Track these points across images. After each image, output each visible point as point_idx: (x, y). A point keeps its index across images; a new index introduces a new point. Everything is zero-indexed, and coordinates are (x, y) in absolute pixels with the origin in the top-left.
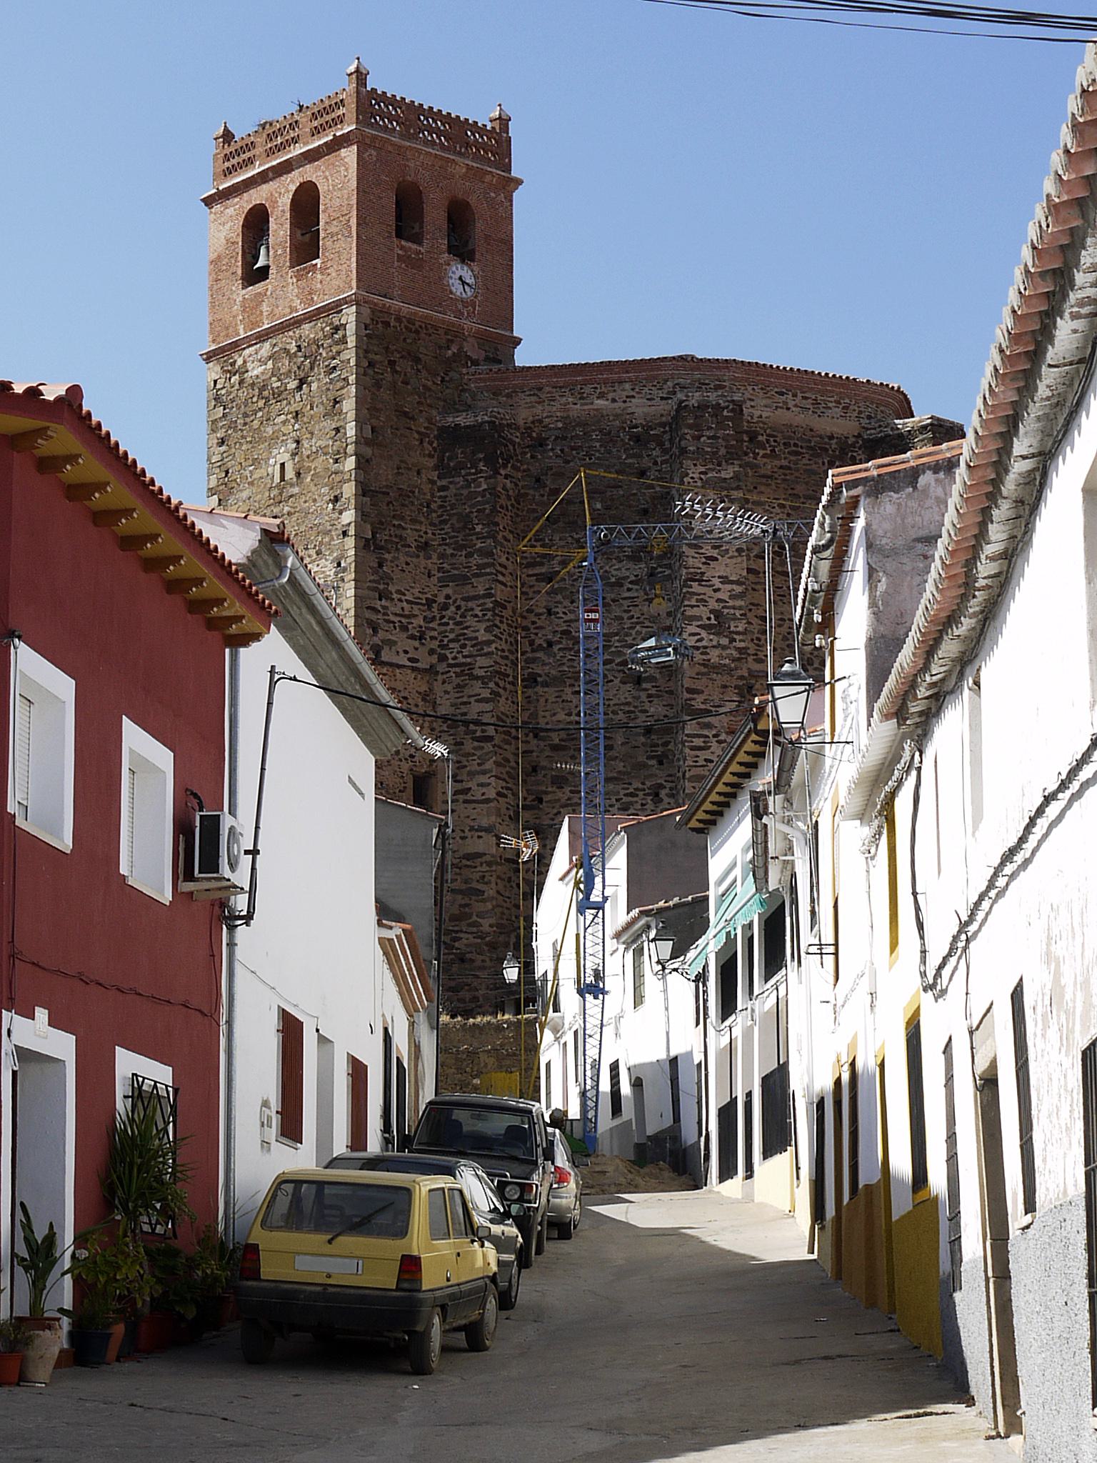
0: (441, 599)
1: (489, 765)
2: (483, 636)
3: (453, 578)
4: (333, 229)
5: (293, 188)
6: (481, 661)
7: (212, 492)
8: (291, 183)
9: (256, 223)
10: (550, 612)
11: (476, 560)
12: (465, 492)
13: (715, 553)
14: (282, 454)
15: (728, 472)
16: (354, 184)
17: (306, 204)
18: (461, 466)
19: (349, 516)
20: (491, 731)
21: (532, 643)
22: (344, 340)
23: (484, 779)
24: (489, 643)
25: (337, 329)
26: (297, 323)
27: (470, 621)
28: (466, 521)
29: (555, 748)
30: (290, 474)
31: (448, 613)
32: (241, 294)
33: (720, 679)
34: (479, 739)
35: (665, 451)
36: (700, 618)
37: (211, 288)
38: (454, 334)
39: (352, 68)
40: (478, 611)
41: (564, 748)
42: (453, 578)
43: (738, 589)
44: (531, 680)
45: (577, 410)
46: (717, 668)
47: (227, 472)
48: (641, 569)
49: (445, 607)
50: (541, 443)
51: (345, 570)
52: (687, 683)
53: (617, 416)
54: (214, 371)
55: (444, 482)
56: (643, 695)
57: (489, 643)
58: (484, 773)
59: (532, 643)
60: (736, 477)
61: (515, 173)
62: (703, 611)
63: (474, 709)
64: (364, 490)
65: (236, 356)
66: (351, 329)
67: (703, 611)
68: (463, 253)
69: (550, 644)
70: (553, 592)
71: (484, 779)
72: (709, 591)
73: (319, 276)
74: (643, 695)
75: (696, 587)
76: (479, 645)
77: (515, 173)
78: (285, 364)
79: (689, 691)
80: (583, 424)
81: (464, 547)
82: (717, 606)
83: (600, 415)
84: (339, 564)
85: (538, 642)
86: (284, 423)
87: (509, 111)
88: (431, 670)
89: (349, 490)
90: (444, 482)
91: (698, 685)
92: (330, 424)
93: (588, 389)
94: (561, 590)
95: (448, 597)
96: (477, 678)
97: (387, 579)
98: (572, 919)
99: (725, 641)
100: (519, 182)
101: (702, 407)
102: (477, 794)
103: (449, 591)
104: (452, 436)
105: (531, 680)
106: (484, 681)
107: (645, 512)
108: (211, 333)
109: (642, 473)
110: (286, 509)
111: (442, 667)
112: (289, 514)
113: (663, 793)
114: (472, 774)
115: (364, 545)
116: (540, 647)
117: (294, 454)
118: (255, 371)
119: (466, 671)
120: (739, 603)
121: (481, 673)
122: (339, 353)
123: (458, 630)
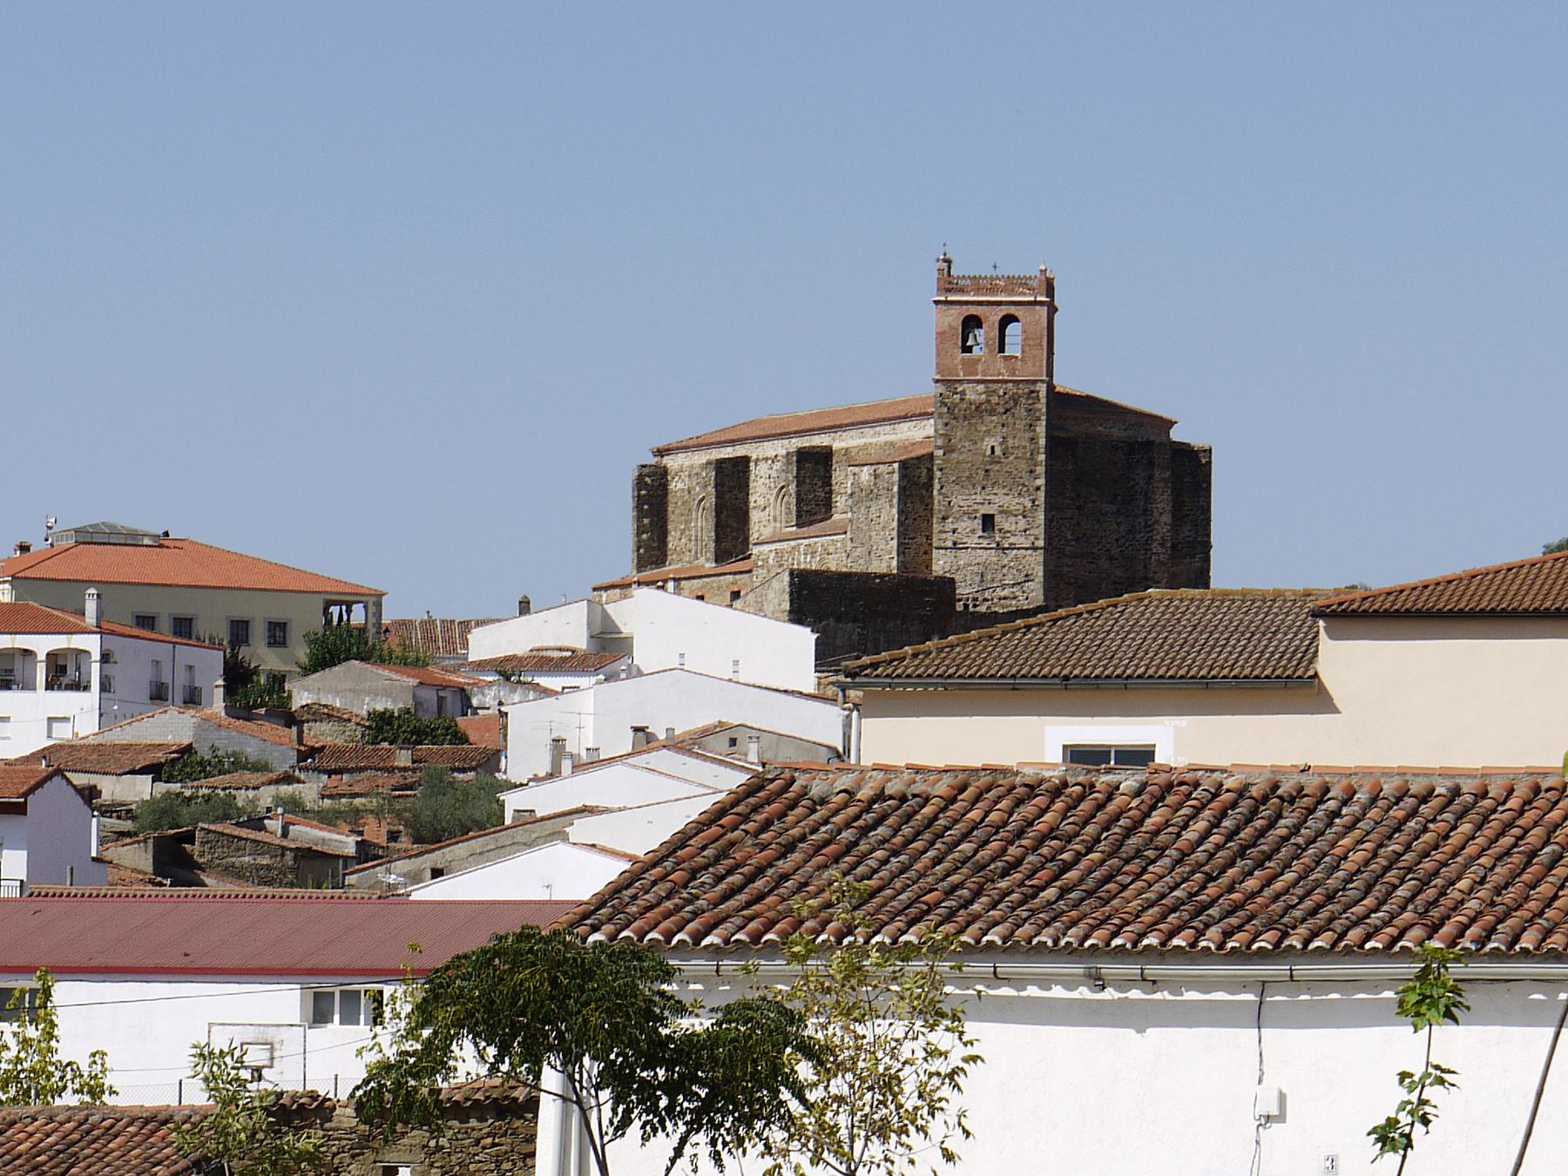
8: (1004, 311)
9: (972, 323)
11: (1067, 501)
19: (1041, 482)
22: (1038, 398)
26: (1006, 382)
30: (998, 452)
45: (1091, 430)
48: (1113, 508)
54: (941, 389)
89: (1041, 470)
92: (1028, 435)
118: (970, 396)
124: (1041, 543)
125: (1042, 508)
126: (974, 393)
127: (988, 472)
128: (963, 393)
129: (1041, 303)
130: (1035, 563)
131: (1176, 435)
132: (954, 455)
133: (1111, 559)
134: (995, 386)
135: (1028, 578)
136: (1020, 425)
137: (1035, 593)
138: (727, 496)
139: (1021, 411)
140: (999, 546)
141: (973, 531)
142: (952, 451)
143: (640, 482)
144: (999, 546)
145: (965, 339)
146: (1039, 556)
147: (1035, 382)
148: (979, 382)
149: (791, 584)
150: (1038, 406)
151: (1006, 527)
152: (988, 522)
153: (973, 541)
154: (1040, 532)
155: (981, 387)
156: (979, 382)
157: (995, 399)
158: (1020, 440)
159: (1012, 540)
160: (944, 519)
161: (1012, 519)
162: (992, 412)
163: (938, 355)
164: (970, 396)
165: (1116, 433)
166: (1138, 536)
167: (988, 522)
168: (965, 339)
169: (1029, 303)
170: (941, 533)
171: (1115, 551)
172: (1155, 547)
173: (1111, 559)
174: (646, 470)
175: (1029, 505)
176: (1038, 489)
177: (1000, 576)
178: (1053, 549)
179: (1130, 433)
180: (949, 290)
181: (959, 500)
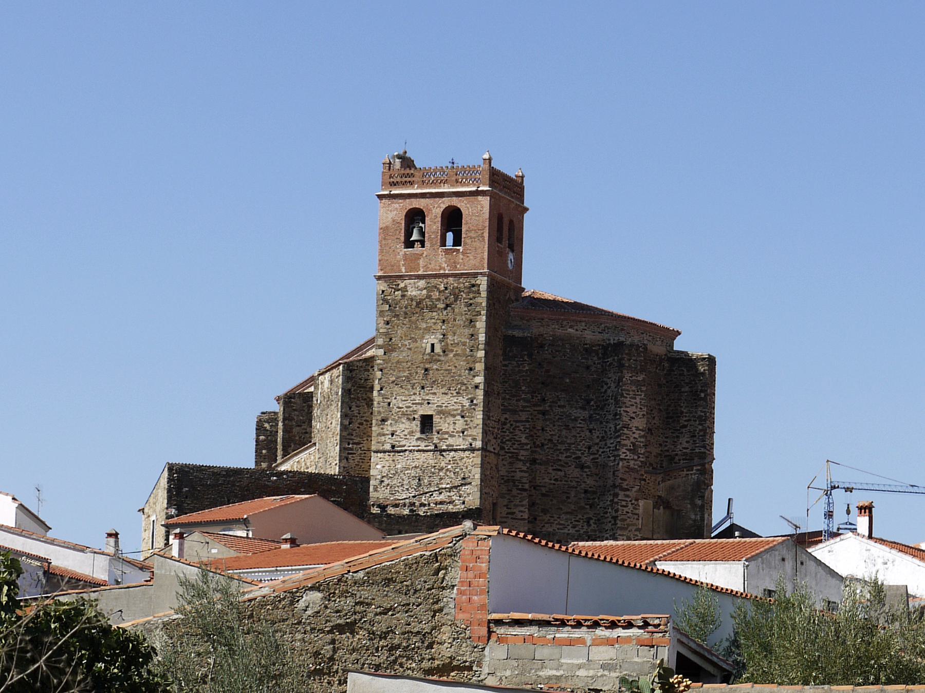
0: (503, 420)
1: (524, 503)
2: (524, 440)
3: (510, 410)
4: (472, 234)
5: (444, 206)
6: (522, 452)
8: (445, 203)
9: (415, 217)
10: (543, 429)
11: (522, 403)
12: (517, 369)
13: (633, 415)
16: (487, 215)
19: (480, 379)
20: (527, 486)
21: (534, 443)
22: (479, 292)
23: (522, 509)
24: (527, 444)
25: (473, 286)
26: (446, 276)
27: (517, 432)
29: (543, 495)
30: (438, 349)
31: (506, 427)
32: (403, 251)
33: (634, 475)
34: (520, 490)
35: (599, 359)
36: (626, 445)
37: (380, 242)
39: (486, 156)
40: (522, 428)
41: (548, 496)
42: (510, 410)
43: (642, 433)
44: (534, 461)
45: (560, 332)
46: (632, 470)
47: (391, 339)
48: (586, 414)
49: (505, 424)
50: (542, 346)
51: (476, 405)
52: (620, 476)
53: (578, 338)
54: (383, 286)
55: (506, 363)
56: (585, 475)
57: (527, 444)
58: (522, 506)
59: (534, 443)
60: (644, 380)
61: (526, 205)
62: (627, 442)
63: (518, 475)
64: (487, 368)
65: (399, 282)
67: (627, 442)
68: (511, 247)
69: (543, 445)
70: (546, 420)
71: (522, 509)
72: (631, 433)
73: (461, 256)
74: (585, 475)
75: (626, 431)
76: (521, 444)
77: (526, 205)
78: (435, 295)
79: (621, 479)
80: (562, 340)
81: (514, 396)
82: (634, 441)
84: (472, 401)
85: (538, 443)
86: (435, 324)
87: (457, 143)
89: (480, 367)
90: (506, 363)
91: (625, 477)
92: (467, 331)
93: (565, 323)
94: (550, 419)
95: (506, 419)
96: (520, 460)
99: (636, 457)
100: (527, 209)
101: (632, 345)
102: (519, 515)
103: (507, 416)
105: (534, 461)
106: (524, 462)
107: (588, 386)
108: (380, 265)
109: (588, 367)
110: (435, 367)
111: (502, 453)
112: (437, 370)
113: (592, 522)
114: (516, 506)
115: (487, 394)
116: (538, 446)
117: (441, 341)
118: (412, 292)
119: (515, 457)
120: (642, 440)
121: (523, 458)
122: (475, 298)
123: (511, 436)
124: (478, 444)
125: (480, 408)
126: (416, 289)
127: (427, 372)
128: (405, 289)
129: (483, 193)
130: (472, 465)
131: (679, 345)
132: (394, 354)
133: (582, 467)
134: (434, 281)
135: (465, 482)
136: (460, 321)
137: (472, 497)
138: (296, 430)
139: (460, 307)
140: (437, 450)
141: (411, 433)
142: (393, 350)
143: (260, 428)
144: (437, 450)
145: (409, 234)
146: (477, 458)
147: (475, 275)
148: (420, 277)
149: (170, 480)
150: (479, 300)
151: (444, 427)
152: (427, 423)
153: (411, 443)
154: (478, 432)
155: (422, 283)
156: (420, 277)
157: (435, 295)
158: (460, 336)
159: (451, 441)
160: (384, 420)
161: (450, 420)
162: (432, 308)
163: (381, 251)
164: (412, 292)
165: (590, 336)
166: (609, 442)
167: (427, 423)
168: (409, 234)
169: (471, 194)
170: (380, 437)
171: (586, 459)
172: (623, 453)
173: (582, 467)
174: (266, 417)
175: (467, 404)
176: (477, 387)
177: (436, 480)
178: (497, 447)
179: (606, 336)
180: (393, 184)
181: (399, 401)
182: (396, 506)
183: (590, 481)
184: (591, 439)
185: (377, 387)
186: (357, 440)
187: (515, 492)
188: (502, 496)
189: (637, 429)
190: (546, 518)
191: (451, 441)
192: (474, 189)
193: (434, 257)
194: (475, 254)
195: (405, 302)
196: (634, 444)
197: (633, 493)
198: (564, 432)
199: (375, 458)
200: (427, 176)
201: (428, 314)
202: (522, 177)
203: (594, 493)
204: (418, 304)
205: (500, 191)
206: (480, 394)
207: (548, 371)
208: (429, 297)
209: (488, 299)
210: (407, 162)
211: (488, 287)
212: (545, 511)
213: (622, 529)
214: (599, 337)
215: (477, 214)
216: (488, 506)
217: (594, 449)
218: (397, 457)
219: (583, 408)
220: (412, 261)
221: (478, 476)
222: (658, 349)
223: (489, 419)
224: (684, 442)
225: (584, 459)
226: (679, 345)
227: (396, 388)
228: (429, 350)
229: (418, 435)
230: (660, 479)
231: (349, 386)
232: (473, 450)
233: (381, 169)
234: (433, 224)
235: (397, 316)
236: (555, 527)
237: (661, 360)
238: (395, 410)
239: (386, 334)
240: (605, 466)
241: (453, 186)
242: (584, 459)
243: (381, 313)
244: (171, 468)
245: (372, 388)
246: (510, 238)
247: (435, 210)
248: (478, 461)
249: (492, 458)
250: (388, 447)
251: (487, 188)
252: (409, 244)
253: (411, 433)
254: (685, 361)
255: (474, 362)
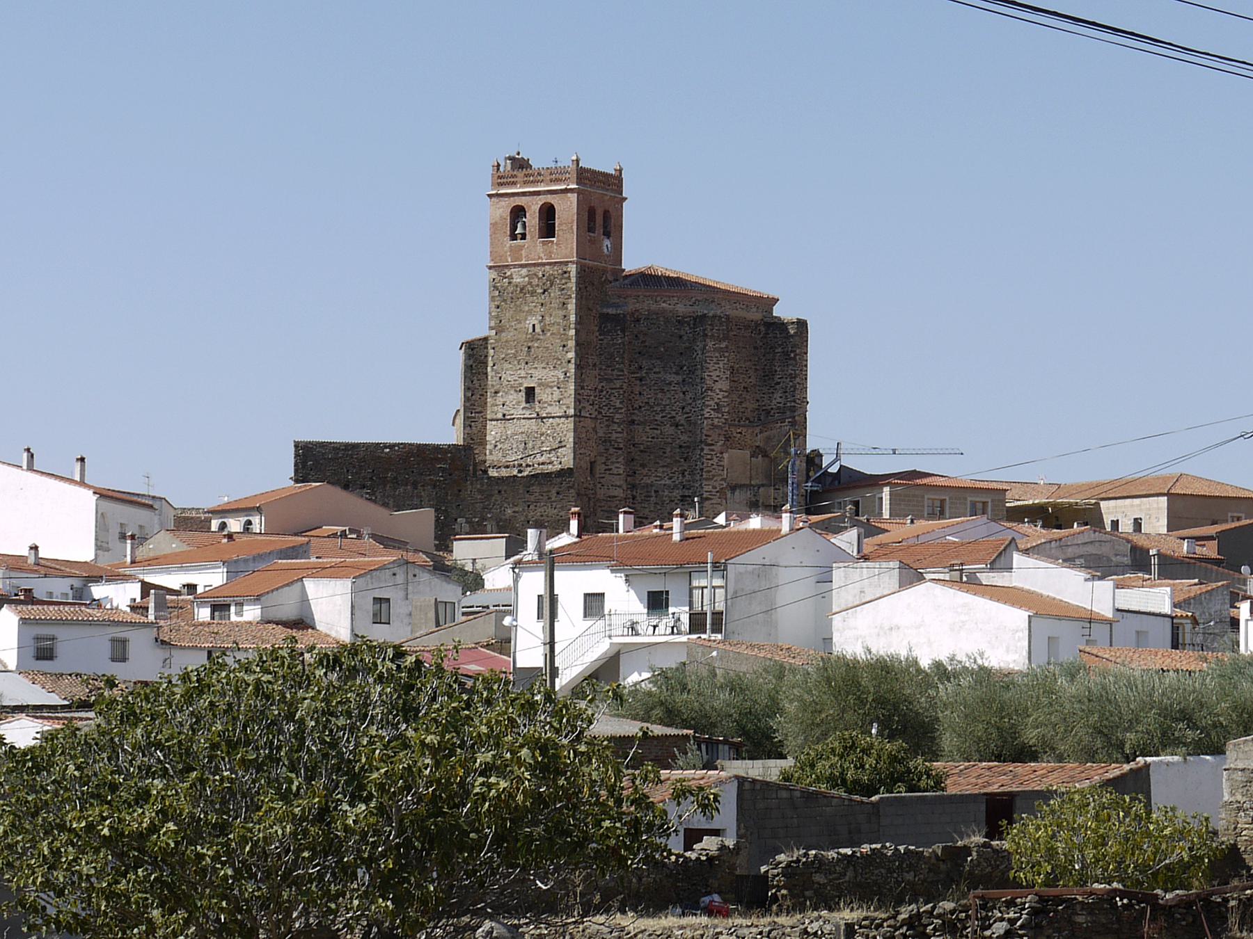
1: (620, 459)
2: (618, 405)
4: (564, 227)
6: (617, 416)
7: (491, 328)
8: (541, 200)
14: (533, 320)
15: (723, 345)
17: (548, 213)
18: (609, 331)
19: (571, 355)
22: (569, 278)
26: (544, 264)
28: (612, 356)
30: (538, 329)
38: (604, 271)
45: (654, 307)
46: (717, 427)
48: (680, 378)
50: (638, 320)
54: (494, 274)
63: (614, 436)
64: (577, 344)
66: (573, 274)
68: (607, 234)
78: (535, 281)
83: (664, 310)
87: (501, 154)
88: (596, 418)
89: (571, 344)
92: (562, 313)
97: (583, 381)
98: (783, 532)
101: (714, 316)
104: (605, 318)
115: (578, 367)
118: (517, 280)
119: (611, 420)
124: (572, 412)
126: (519, 276)
127: (529, 351)
128: (511, 277)
129: (571, 190)
131: (777, 311)
139: (555, 292)
140: (539, 417)
141: (518, 403)
144: (539, 417)
145: (514, 228)
146: (570, 424)
147: (566, 263)
148: (522, 266)
150: (569, 285)
151: (544, 397)
152: (530, 393)
153: (518, 412)
154: (571, 401)
155: (524, 271)
156: (522, 266)
157: (535, 281)
159: (549, 409)
161: (549, 390)
162: (533, 293)
163: (492, 244)
167: (530, 393)
168: (514, 228)
169: (563, 191)
170: (494, 408)
171: (680, 418)
180: (501, 184)
182: (507, 467)
183: (684, 438)
184: (684, 400)
185: (490, 364)
186: (479, 409)
187: (612, 451)
188: (601, 454)
189: (721, 390)
190: (645, 471)
191: (549, 409)
192: (564, 187)
193: (534, 248)
194: (566, 245)
195: (511, 289)
196: (717, 404)
197: (717, 448)
198: (660, 396)
199: (490, 425)
200: (537, 177)
201: (530, 299)
202: (620, 171)
203: (689, 447)
204: (522, 289)
205: (591, 186)
206: (572, 367)
207: (643, 342)
208: (530, 283)
209: (578, 283)
210: (520, 164)
211: (578, 273)
212: (643, 466)
213: (707, 479)
214: (691, 309)
215: (567, 210)
216: (585, 465)
217: (687, 410)
218: (508, 424)
219: (677, 373)
220: (516, 252)
221: (571, 440)
222: (755, 315)
223: (582, 388)
224: (778, 397)
225: (678, 418)
226: (777, 311)
227: (506, 365)
228: (531, 330)
229: (524, 405)
230: (758, 430)
231: (471, 362)
232: (567, 417)
233: (490, 171)
234: (532, 220)
235: (504, 301)
236: (653, 479)
237: (757, 325)
238: (505, 383)
239: (497, 317)
240: (695, 424)
241: (548, 185)
242: (678, 418)
243: (493, 299)
244: (297, 445)
245: (486, 364)
246: (605, 227)
247: (534, 208)
248: (571, 426)
249: (589, 423)
250: (500, 416)
251: (575, 186)
252: (513, 237)
253: (518, 403)
254: (779, 326)
255: (567, 340)
